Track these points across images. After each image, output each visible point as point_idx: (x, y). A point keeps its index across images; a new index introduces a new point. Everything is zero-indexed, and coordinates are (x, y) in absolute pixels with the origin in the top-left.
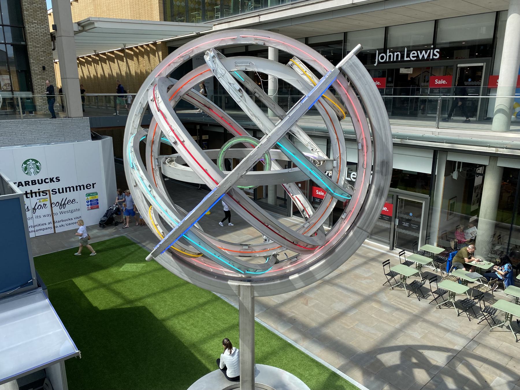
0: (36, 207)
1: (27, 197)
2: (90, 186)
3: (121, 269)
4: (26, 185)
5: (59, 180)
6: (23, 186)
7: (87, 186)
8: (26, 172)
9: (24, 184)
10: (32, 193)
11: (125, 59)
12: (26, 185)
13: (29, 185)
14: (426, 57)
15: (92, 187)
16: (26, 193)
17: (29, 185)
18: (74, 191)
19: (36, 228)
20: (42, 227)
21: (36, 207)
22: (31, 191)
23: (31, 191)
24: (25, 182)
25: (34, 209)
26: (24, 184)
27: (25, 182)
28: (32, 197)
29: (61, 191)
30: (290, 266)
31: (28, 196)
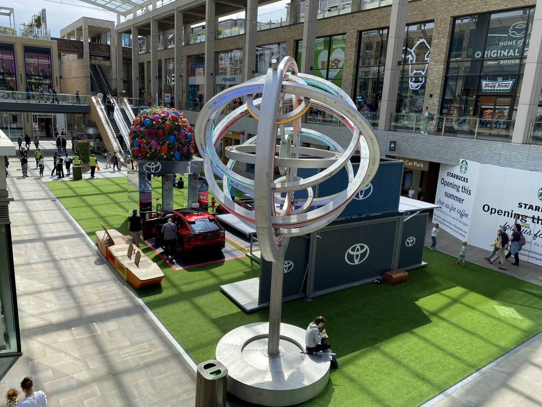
0: (538, 235)
1: (533, 222)
2: (502, 212)
3: (496, 307)
4: (535, 210)
5: (519, 204)
6: (533, 210)
7: (498, 212)
8: (541, 198)
9: (534, 208)
10: (538, 219)
11: (470, 59)
12: (535, 210)
13: (539, 211)
14: (512, 51)
15: (503, 214)
16: (533, 218)
17: (539, 211)
18: (508, 216)
19: (531, 254)
20: (537, 256)
21: (538, 235)
22: (539, 217)
23: (539, 217)
24: (536, 207)
25: (535, 235)
26: (534, 208)
27: (536, 207)
28: (538, 223)
29: (507, 214)
30: (93, 244)
31: (535, 221)
